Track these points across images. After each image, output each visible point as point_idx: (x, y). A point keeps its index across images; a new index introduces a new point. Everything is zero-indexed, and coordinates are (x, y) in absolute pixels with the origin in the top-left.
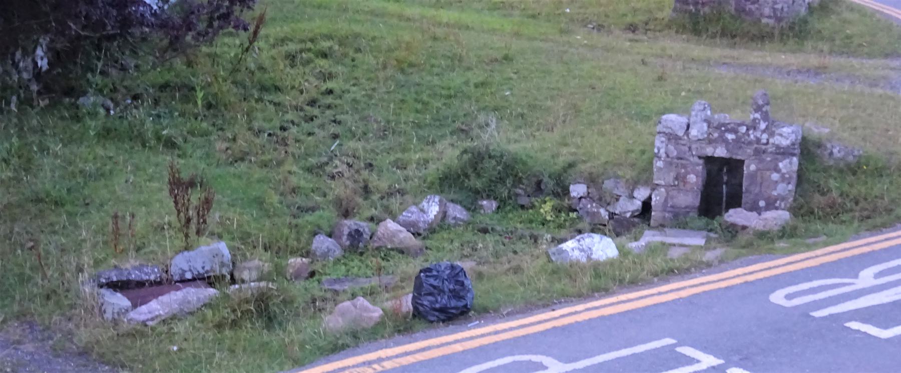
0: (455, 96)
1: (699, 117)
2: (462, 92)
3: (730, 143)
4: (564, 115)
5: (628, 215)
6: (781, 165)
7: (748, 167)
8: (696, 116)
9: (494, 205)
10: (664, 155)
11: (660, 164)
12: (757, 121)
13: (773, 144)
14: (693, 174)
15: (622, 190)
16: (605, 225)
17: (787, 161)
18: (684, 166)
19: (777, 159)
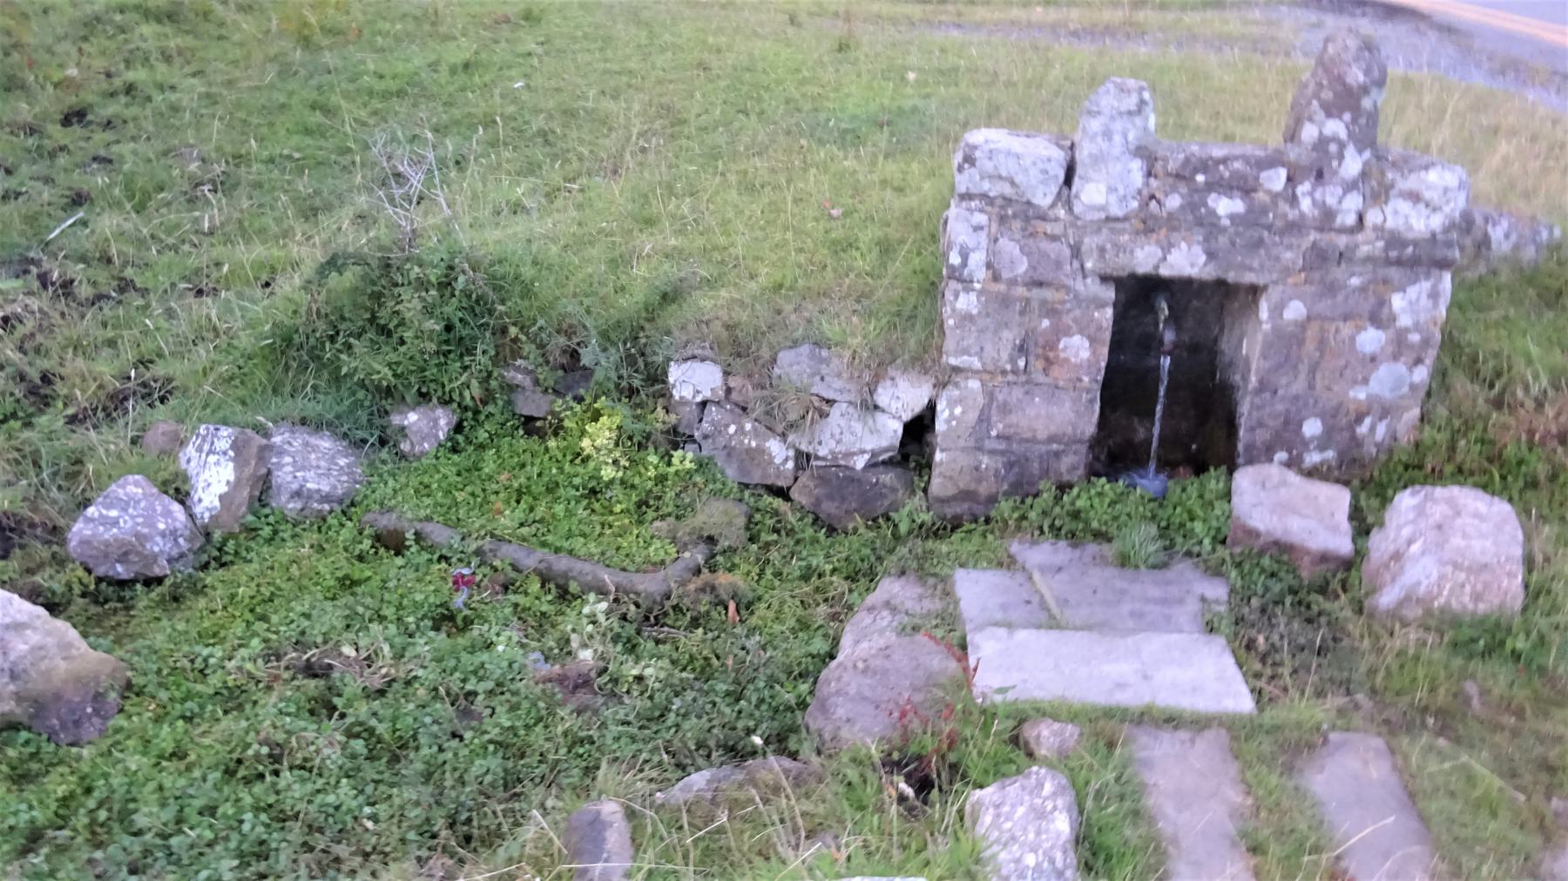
0: (400, 93)
1: (1117, 138)
2: (419, 84)
3: (1224, 230)
4: (641, 135)
5: (860, 463)
6: (1397, 302)
7: (1277, 310)
8: (1107, 134)
9: (444, 420)
10: (981, 274)
11: (967, 302)
12: (1333, 148)
13: (1379, 229)
14: (1081, 332)
15: (838, 384)
16: (782, 493)
17: (1425, 286)
18: (1051, 311)
19: (1385, 282)
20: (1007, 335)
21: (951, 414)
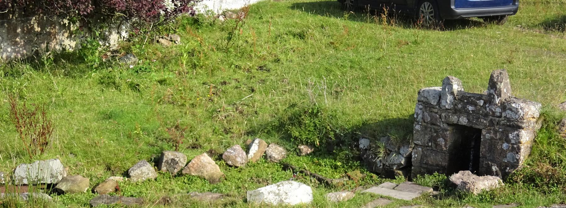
20: (427, 137)
21: (415, 156)
